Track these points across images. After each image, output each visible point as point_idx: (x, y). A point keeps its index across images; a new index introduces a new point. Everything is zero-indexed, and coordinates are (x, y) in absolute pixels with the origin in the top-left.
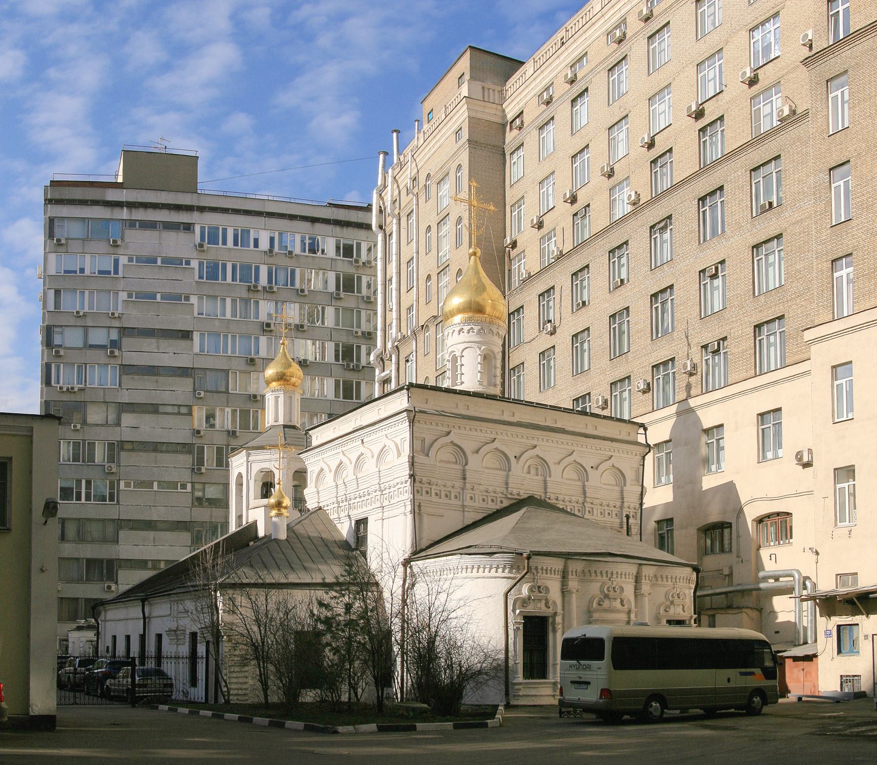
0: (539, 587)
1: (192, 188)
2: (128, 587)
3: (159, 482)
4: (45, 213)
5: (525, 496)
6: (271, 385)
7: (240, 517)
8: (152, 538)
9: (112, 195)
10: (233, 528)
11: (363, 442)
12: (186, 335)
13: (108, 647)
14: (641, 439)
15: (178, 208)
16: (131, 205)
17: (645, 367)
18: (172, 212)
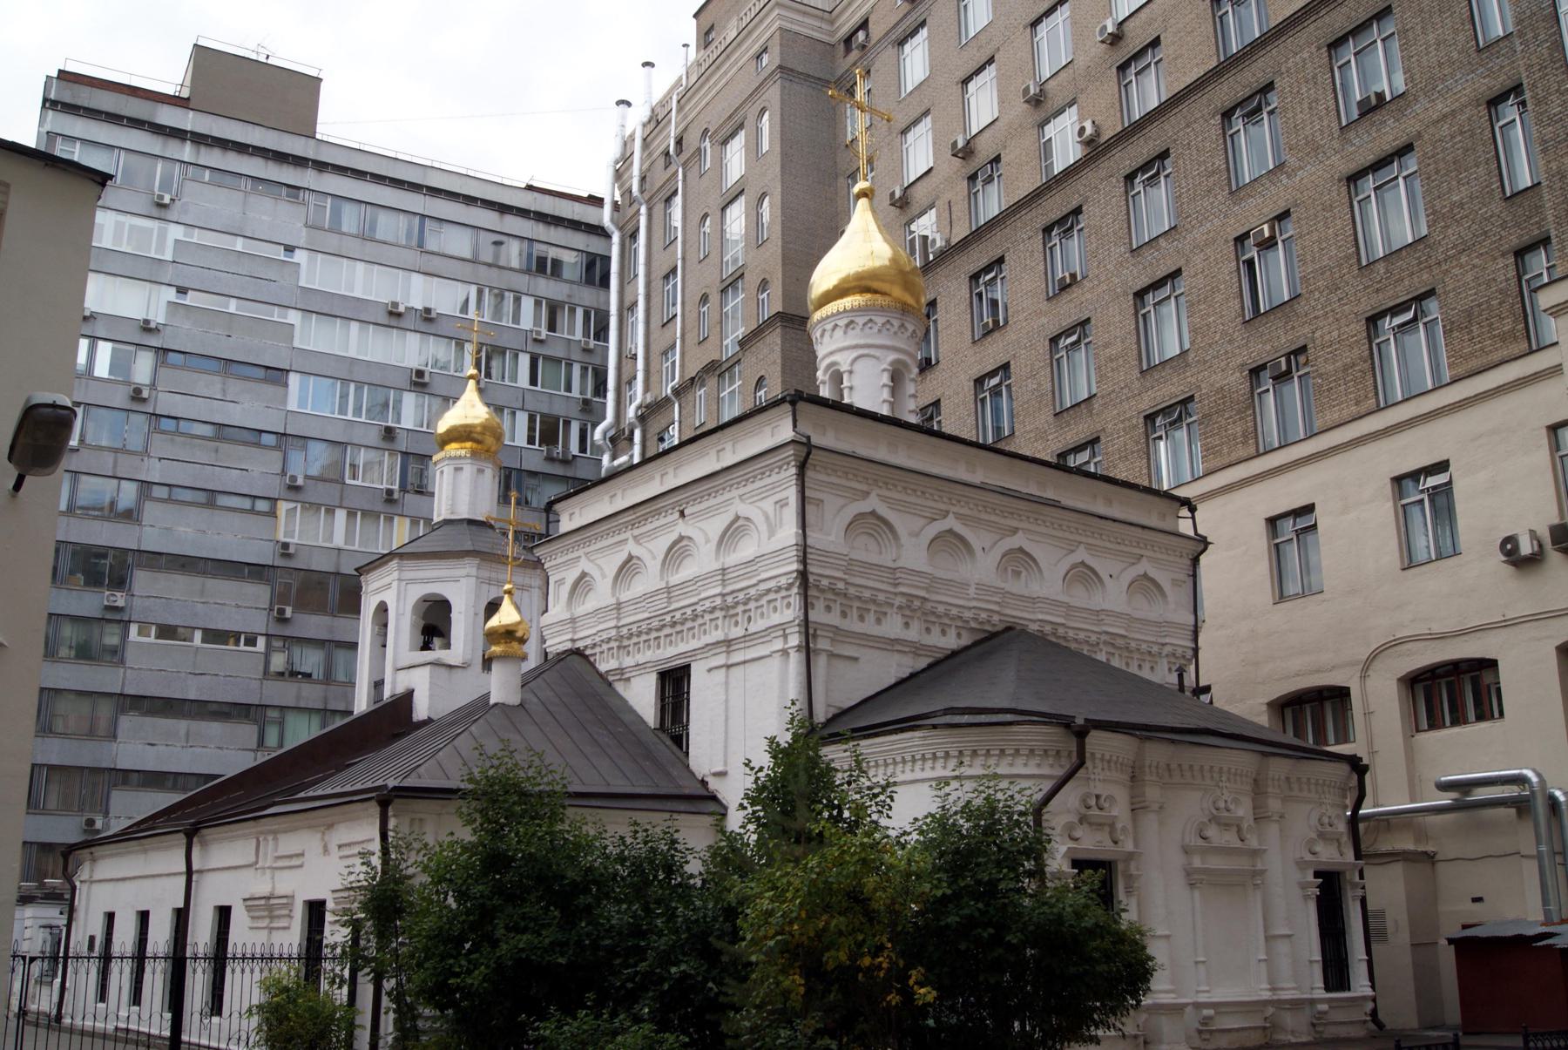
0: (1098, 797)
1: (307, 128)
2: (126, 823)
3: (206, 631)
4: (41, 124)
5: (1000, 627)
6: (448, 448)
7: (378, 685)
8: (182, 732)
9: (168, 116)
10: (361, 703)
11: (682, 514)
12: (276, 375)
13: (92, 939)
14: (1185, 527)
15: (281, 157)
16: (200, 139)
17: (1129, 419)
18: (271, 164)
